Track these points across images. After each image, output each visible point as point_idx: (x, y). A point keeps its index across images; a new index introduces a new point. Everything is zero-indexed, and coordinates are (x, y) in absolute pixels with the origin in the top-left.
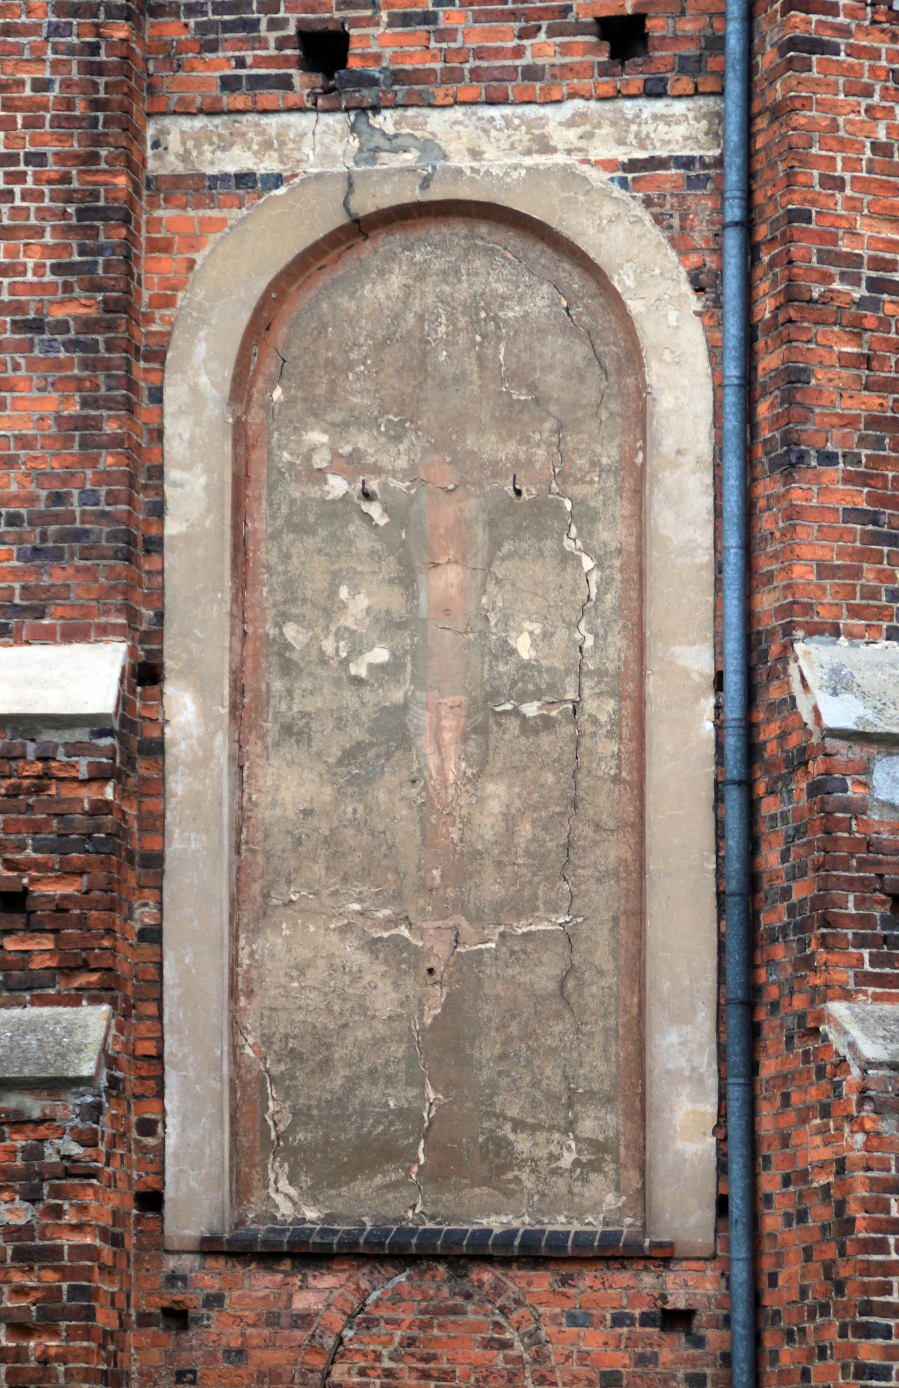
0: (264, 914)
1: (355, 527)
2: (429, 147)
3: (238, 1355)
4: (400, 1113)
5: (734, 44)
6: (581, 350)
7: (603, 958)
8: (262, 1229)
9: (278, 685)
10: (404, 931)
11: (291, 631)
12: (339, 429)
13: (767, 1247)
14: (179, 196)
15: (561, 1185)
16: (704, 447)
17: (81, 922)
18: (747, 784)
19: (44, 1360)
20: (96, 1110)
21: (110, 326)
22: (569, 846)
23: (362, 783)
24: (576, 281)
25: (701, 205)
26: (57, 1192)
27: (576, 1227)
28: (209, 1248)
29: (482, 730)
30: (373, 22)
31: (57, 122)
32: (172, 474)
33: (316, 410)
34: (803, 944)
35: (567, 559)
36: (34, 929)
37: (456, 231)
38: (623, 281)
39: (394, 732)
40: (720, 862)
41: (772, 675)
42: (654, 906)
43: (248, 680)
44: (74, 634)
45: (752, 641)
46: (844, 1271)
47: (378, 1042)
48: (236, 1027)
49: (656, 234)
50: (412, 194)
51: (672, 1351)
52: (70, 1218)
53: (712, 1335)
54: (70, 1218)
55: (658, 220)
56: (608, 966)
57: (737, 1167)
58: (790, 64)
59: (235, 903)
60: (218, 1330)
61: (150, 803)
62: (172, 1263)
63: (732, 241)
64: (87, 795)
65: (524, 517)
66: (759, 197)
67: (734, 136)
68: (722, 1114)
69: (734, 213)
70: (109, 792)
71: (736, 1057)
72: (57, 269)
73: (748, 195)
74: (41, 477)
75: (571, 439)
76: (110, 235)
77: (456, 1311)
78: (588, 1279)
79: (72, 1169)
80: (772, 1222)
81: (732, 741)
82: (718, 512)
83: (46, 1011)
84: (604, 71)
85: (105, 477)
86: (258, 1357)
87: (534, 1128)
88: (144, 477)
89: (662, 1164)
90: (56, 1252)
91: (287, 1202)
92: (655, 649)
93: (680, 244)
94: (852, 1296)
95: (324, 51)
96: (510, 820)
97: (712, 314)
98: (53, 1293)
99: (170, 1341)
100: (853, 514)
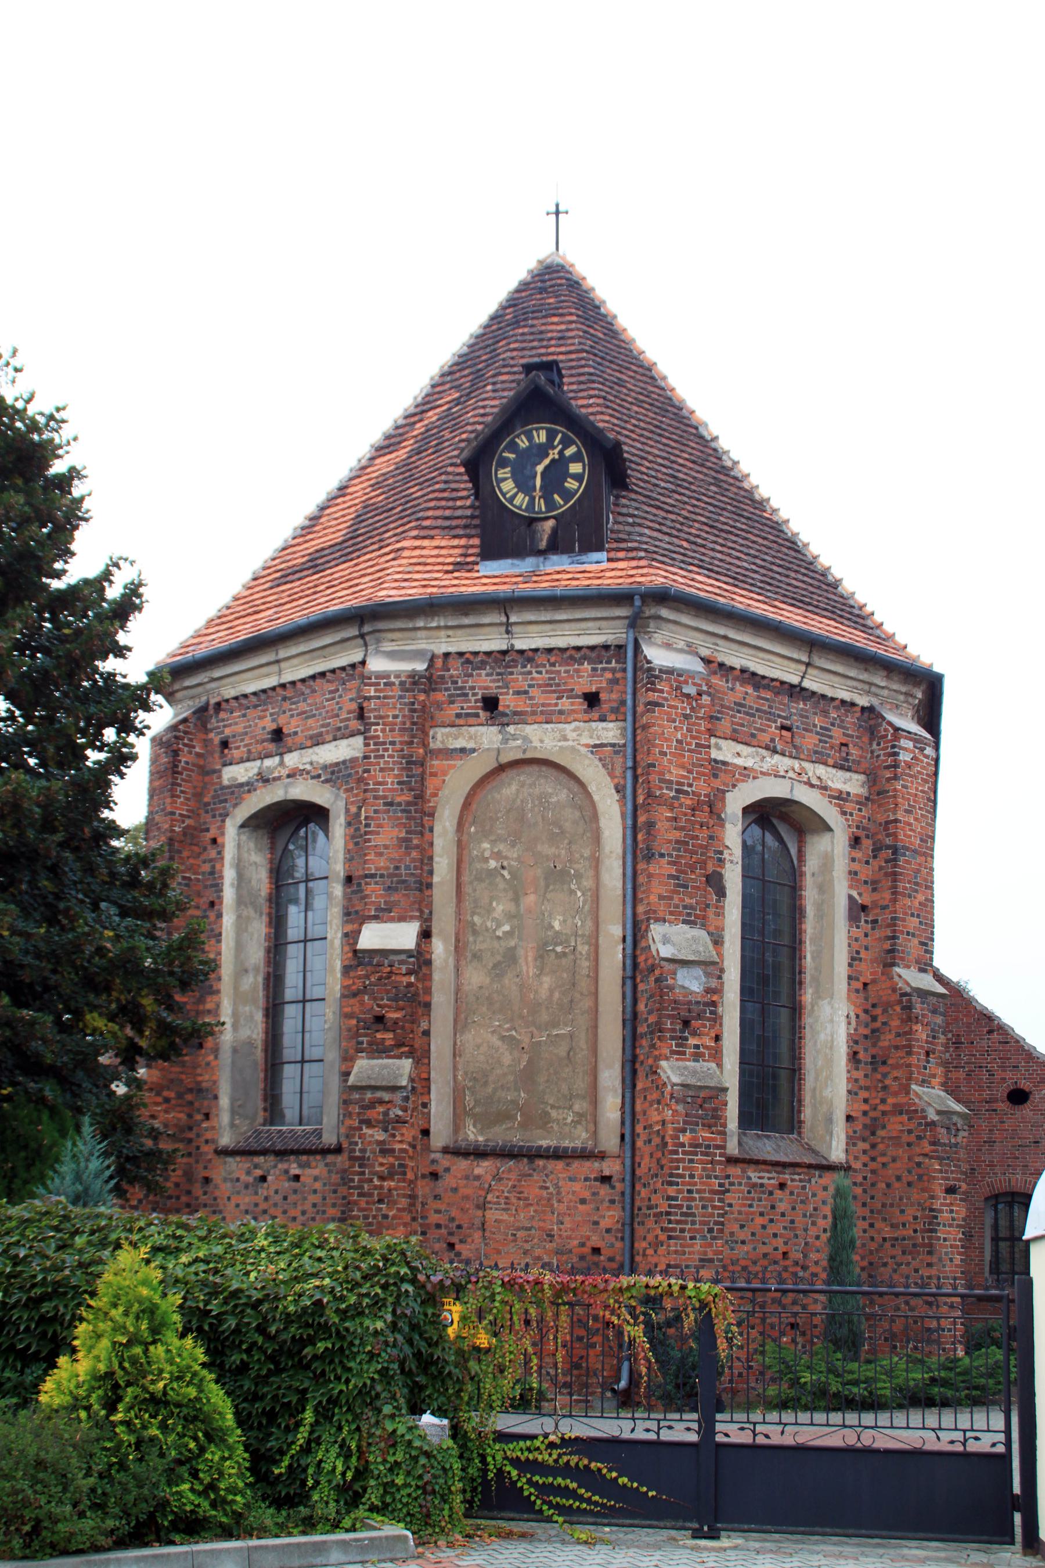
0: (465, 1026)
1: (499, 879)
2: (526, 739)
3: (455, 1190)
4: (512, 1101)
5: (629, 702)
6: (577, 814)
7: (583, 1044)
8: (463, 1144)
9: (471, 939)
10: (514, 1033)
11: (476, 919)
12: (493, 842)
13: (638, 1153)
14: (441, 756)
15: (567, 1129)
16: (619, 850)
17: (403, 1028)
18: (633, 978)
19: (390, 1190)
20: (406, 1099)
21: (416, 804)
22: (571, 1001)
23: (500, 976)
24: (576, 788)
25: (619, 760)
26: (394, 1128)
27: (572, 1145)
28: (446, 1150)
29: (541, 957)
30: (507, 694)
31: (400, 730)
32: (436, 859)
33: (485, 834)
34: (652, 1039)
35: (572, 892)
36: (387, 1030)
37: (535, 768)
38: (592, 788)
39: (511, 957)
40: (624, 1008)
41: (643, 937)
42: (601, 1025)
43: (461, 937)
44: (402, 919)
45: (635, 924)
46: (664, 1162)
47: (505, 1075)
48: (455, 1068)
49: (603, 771)
50: (520, 756)
51: (604, 1190)
52: (398, 1138)
53: (617, 1185)
54: (398, 1138)
55: (604, 766)
56: (584, 1047)
57: (628, 1123)
58: (648, 711)
59: (455, 1021)
60: (448, 1181)
61: (427, 983)
62: (433, 1156)
63: (629, 774)
64: (405, 980)
65: (557, 876)
66: (638, 758)
67: (630, 736)
68: (623, 1103)
69: (630, 764)
70: (413, 979)
71: (628, 1082)
72: (399, 783)
73: (635, 757)
74: (392, 860)
75: (574, 847)
76: (417, 771)
77: (530, 1175)
78: (576, 1164)
79: (399, 1120)
80: (639, 1143)
81: (629, 962)
82: (624, 875)
83: (390, 1061)
84: (586, 712)
85: (413, 860)
86: (463, 1191)
87: (559, 1108)
88: (427, 860)
89: (602, 1125)
90: (393, 1151)
91: (473, 1134)
92: (602, 927)
93: (612, 775)
94: (666, 1171)
95: (490, 704)
96: (551, 991)
97: (622, 801)
98: (392, 1165)
99: (432, 1184)
100: (671, 876)
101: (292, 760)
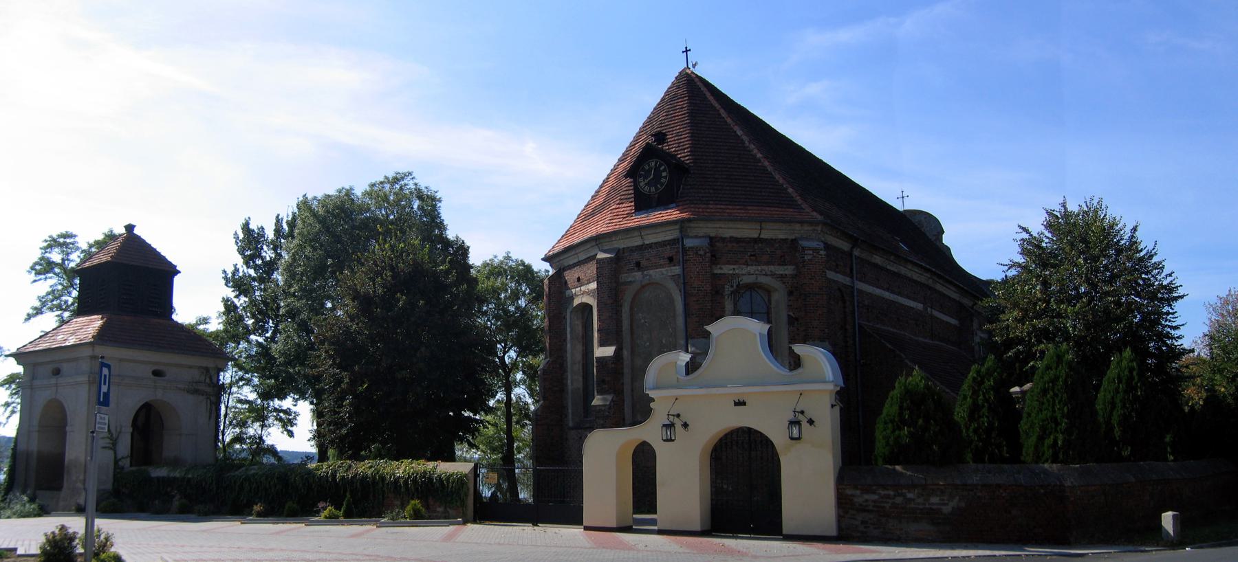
95: (638, 264)
101: (583, 288)
